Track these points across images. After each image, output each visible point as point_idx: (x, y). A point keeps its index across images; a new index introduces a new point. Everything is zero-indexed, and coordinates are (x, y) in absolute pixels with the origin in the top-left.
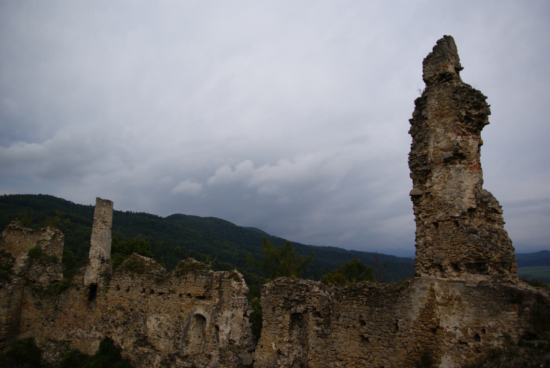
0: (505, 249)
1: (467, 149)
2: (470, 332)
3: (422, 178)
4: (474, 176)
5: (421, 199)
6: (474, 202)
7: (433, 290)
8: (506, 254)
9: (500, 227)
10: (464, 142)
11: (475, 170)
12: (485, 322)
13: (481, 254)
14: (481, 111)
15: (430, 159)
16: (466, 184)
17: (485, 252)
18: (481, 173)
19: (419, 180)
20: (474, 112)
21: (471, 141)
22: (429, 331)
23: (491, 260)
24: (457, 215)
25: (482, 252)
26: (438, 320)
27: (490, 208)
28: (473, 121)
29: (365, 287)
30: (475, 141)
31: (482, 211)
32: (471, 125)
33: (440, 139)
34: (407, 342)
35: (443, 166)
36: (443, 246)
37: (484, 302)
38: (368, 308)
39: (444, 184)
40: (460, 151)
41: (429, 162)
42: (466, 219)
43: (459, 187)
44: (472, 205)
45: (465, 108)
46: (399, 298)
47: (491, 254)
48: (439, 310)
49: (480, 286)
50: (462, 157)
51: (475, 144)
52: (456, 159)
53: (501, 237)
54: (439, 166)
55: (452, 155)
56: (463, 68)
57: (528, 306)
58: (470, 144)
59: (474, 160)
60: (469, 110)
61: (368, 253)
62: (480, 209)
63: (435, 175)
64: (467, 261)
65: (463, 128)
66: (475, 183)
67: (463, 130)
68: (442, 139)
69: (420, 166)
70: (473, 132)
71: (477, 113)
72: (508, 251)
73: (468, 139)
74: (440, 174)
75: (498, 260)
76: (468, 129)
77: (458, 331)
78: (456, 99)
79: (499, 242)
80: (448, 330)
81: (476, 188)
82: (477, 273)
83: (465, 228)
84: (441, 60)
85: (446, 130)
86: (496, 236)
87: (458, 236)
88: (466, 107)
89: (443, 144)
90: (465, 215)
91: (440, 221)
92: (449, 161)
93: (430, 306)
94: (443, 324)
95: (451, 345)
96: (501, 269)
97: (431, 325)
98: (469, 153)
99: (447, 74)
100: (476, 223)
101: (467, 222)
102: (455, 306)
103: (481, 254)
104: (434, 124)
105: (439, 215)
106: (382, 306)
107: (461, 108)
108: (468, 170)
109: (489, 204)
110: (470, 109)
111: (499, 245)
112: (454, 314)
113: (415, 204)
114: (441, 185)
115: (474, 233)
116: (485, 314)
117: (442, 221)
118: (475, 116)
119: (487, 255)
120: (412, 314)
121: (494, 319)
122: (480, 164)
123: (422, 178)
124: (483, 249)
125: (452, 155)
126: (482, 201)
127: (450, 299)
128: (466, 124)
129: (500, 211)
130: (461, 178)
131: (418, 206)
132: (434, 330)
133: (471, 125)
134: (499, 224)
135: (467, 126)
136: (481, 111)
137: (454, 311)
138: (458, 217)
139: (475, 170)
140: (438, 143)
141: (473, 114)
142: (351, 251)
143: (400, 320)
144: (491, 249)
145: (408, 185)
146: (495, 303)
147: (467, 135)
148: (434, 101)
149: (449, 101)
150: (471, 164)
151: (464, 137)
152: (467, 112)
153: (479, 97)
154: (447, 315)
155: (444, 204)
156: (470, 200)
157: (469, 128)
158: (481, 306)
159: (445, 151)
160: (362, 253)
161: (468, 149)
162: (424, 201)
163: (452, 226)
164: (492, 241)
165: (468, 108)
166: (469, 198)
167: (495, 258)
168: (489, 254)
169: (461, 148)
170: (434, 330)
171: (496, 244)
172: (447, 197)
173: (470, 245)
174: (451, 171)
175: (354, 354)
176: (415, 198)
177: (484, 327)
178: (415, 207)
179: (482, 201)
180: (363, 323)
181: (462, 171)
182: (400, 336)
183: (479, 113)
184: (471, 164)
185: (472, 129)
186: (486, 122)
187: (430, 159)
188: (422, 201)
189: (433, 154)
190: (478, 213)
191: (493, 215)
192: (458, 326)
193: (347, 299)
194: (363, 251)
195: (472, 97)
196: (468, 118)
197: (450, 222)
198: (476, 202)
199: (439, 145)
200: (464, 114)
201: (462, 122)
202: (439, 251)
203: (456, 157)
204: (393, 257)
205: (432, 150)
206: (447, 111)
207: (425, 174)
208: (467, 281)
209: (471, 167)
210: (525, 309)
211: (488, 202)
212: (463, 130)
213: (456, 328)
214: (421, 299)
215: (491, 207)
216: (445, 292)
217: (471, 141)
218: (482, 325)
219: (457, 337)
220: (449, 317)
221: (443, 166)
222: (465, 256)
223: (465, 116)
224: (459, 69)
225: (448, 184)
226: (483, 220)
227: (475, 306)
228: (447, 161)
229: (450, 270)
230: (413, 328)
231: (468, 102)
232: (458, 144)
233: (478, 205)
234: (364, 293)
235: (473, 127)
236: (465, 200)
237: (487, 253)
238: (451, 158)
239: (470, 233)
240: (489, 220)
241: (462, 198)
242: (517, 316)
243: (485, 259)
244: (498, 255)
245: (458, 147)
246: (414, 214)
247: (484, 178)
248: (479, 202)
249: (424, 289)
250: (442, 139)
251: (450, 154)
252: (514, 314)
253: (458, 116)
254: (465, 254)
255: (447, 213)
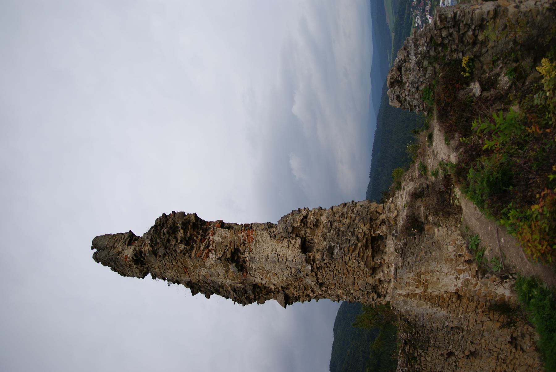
0: (354, 216)
1: (227, 246)
2: (462, 267)
3: (264, 292)
4: (260, 239)
5: (291, 295)
6: (293, 242)
7: (408, 295)
8: (359, 215)
9: (325, 215)
10: (218, 248)
11: (252, 236)
12: (449, 254)
13: (359, 245)
14: (179, 225)
15: (239, 285)
16: (269, 252)
17: (356, 242)
18: (257, 225)
19: (266, 295)
20: (180, 234)
21: (217, 238)
22: (461, 301)
23: (367, 232)
24: (310, 267)
25: (356, 245)
26: (446, 292)
27: (301, 225)
28: (191, 235)
29: (404, 350)
30: (217, 233)
31: (305, 231)
32: (197, 237)
33: (214, 272)
34: (476, 321)
35: (247, 273)
36: (350, 281)
37: (423, 253)
38: (430, 349)
39: (270, 275)
40: (228, 255)
41: (243, 286)
42: (314, 257)
43: (273, 261)
44: (297, 245)
45: (175, 244)
46: (418, 323)
47: (360, 233)
48: (432, 291)
49: (402, 252)
50: (236, 252)
51: (220, 231)
52: (238, 257)
53: (338, 219)
54: (248, 278)
55: (234, 264)
56: (130, 231)
57: (426, 217)
58: (221, 240)
59: (240, 235)
60: (177, 240)
61: (372, 160)
62: (303, 232)
63: (258, 280)
64: (369, 258)
65: (200, 247)
66: (268, 238)
67: (202, 248)
68: (212, 266)
69: (249, 293)
70: (205, 233)
71: (182, 231)
72: (355, 212)
73: (214, 242)
74: (257, 276)
75: (368, 226)
76: (202, 241)
77: (461, 276)
78: (164, 255)
79: (344, 221)
80: (460, 285)
81: (275, 236)
82: (385, 242)
83: (326, 261)
84: (119, 262)
85: (204, 266)
86: (336, 224)
87: (337, 268)
88: (173, 243)
89: (221, 270)
90: (310, 257)
91: (318, 282)
92: (242, 265)
93: (429, 299)
94: (452, 289)
95: (479, 284)
96: (379, 222)
97: (454, 300)
98: (231, 242)
99: (135, 258)
100: (320, 243)
101: (318, 256)
102: (427, 278)
103: (359, 245)
104: (197, 276)
105: (310, 282)
106: (429, 338)
107: (175, 251)
108: (252, 246)
109: (295, 225)
110: (176, 238)
111: (348, 221)
112: (438, 279)
113: (297, 299)
114: (272, 277)
115: (332, 254)
116: (438, 254)
117: (317, 280)
118: (185, 232)
119: (360, 239)
120: (438, 314)
121: (445, 246)
122: (247, 225)
123: (264, 292)
124: (353, 245)
125: (234, 264)
126: (292, 232)
127: (420, 282)
128: (196, 242)
129: (304, 213)
130: (262, 258)
131: (299, 298)
132: (459, 297)
133: (197, 237)
134: (321, 215)
135: (198, 240)
136: (179, 225)
137: (435, 279)
138: (312, 266)
139: (252, 236)
140: (219, 275)
141: (183, 235)
142: (370, 177)
143: (447, 324)
144: (353, 234)
145: (273, 304)
146: (423, 245)
147: (209, 242)
148: (167, 273)
149: (166, 261)
150: (245, 240)
151: (211, 247)
152: (181, 243)
153: (163, 224)
154: (440, 286)
155: (296, 276)
156: (290, 247)
157: (201, 240)
158: (427, 256)
159: (229, 269)
160: (373, 166)
161: (226, 244)
162: (292, 291)
163: (323, 272)
164: (342, 229)
165: (174, 241)
166: (288, 248)
167: (364, 228)
168: (359, 236)
169: (224, 253)
170: (459, 297)
171: (346, 225)
172: (286, 273)
173: (348, 258)
174: (254, 266)
175: (493, 364)
176: (287, 301)
177: (455, 255)
178: (301, 300)
179: (292, 232)
180: (450, 354)
181: (253, 256)
182: (468, 326)
183: (182, 228)
184: (245, 240)
185: (202, 235)
186: (193, 218)
187: (239, 285)
188: (293, 294)
189: (233, 280)
190: (308, 235)
191: (309, 221)
192: (454, 276)
193: (419, 364)
194: (370, 164)
195: (162, 234)
196: (188, 242)
197: (319, 273)
198: (292, 238)
199: (221, 274)
200: (182, 247)
201: (192, 248)
202: (356, 284)
203: (236, 258)
204: (376, 134)
205: (228, 281)
206: (179, 264)
207: (258, 290)
208: (396, 264)
209: (249, 242)
210: (431, 220)
211: (293, 227)
212: (202, 248)
213: (457, 278)
214: (419, 305)
215: (299, 224)
216: (410, 285)
217: (217, 238)
218: (454, 258)
219: (470, 278)
220: (442, 284)
221: (247, 273)
222: (363, 263)
223: (185, 245)
224: (131, 238)
225: (274, 258)
226: (317, 231)
227: (428, 262)
228: (242, 267)
229: (382, 274)
230: (458, 314)
231: (168, 241)
232: (219, 259)
233: (297, 236)
234: (411, 351)
235: (199, 234)
236: (290, 254)
237: (358, 239)
238: (236, 266)
239: (332, 257)
240: (317, 224)
241: (287, 260)
242: (440, 228)
243: (367, 239)
244: (361, 225)
245: (223, 258)
246: (309, 301)
247: (263, 222)
248: (294, 236)
249: (405, 303)
250: (212, 266)
251: (232, 267)
252: (438, 230)
253: (184, 254)
254: (359, 263)
255: (307, 275)
